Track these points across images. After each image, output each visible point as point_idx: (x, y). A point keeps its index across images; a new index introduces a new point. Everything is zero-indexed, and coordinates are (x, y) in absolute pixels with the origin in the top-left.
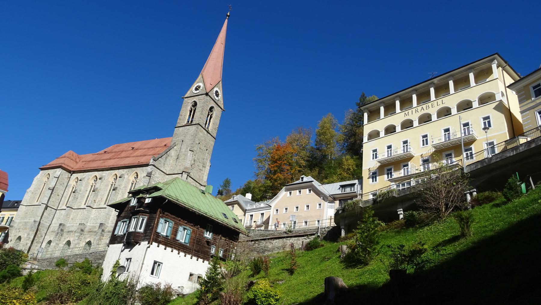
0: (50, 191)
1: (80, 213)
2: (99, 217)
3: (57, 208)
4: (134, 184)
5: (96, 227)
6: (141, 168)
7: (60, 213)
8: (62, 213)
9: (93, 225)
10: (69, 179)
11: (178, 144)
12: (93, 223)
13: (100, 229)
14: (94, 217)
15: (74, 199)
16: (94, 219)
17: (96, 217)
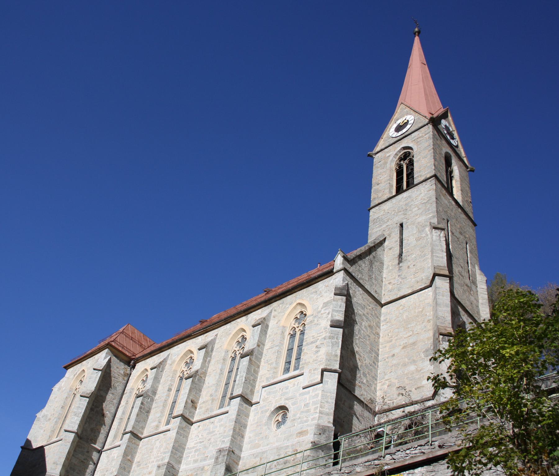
0: (85, 400)
1: (158, 444)
2: (209, 440)
3: (103, 448)
4: (298, 333)
5: (206, 468)
6: (311, 289)
7: (108, 457)
8: (112, 455)
9: (196, 465)
10: (126, 379)
11: (389, 235)
12: (195, 461)
13: (219, 466)
14: (197, 443)
15: (141, 412)
16: (195, 451)
17: (201, 442)
